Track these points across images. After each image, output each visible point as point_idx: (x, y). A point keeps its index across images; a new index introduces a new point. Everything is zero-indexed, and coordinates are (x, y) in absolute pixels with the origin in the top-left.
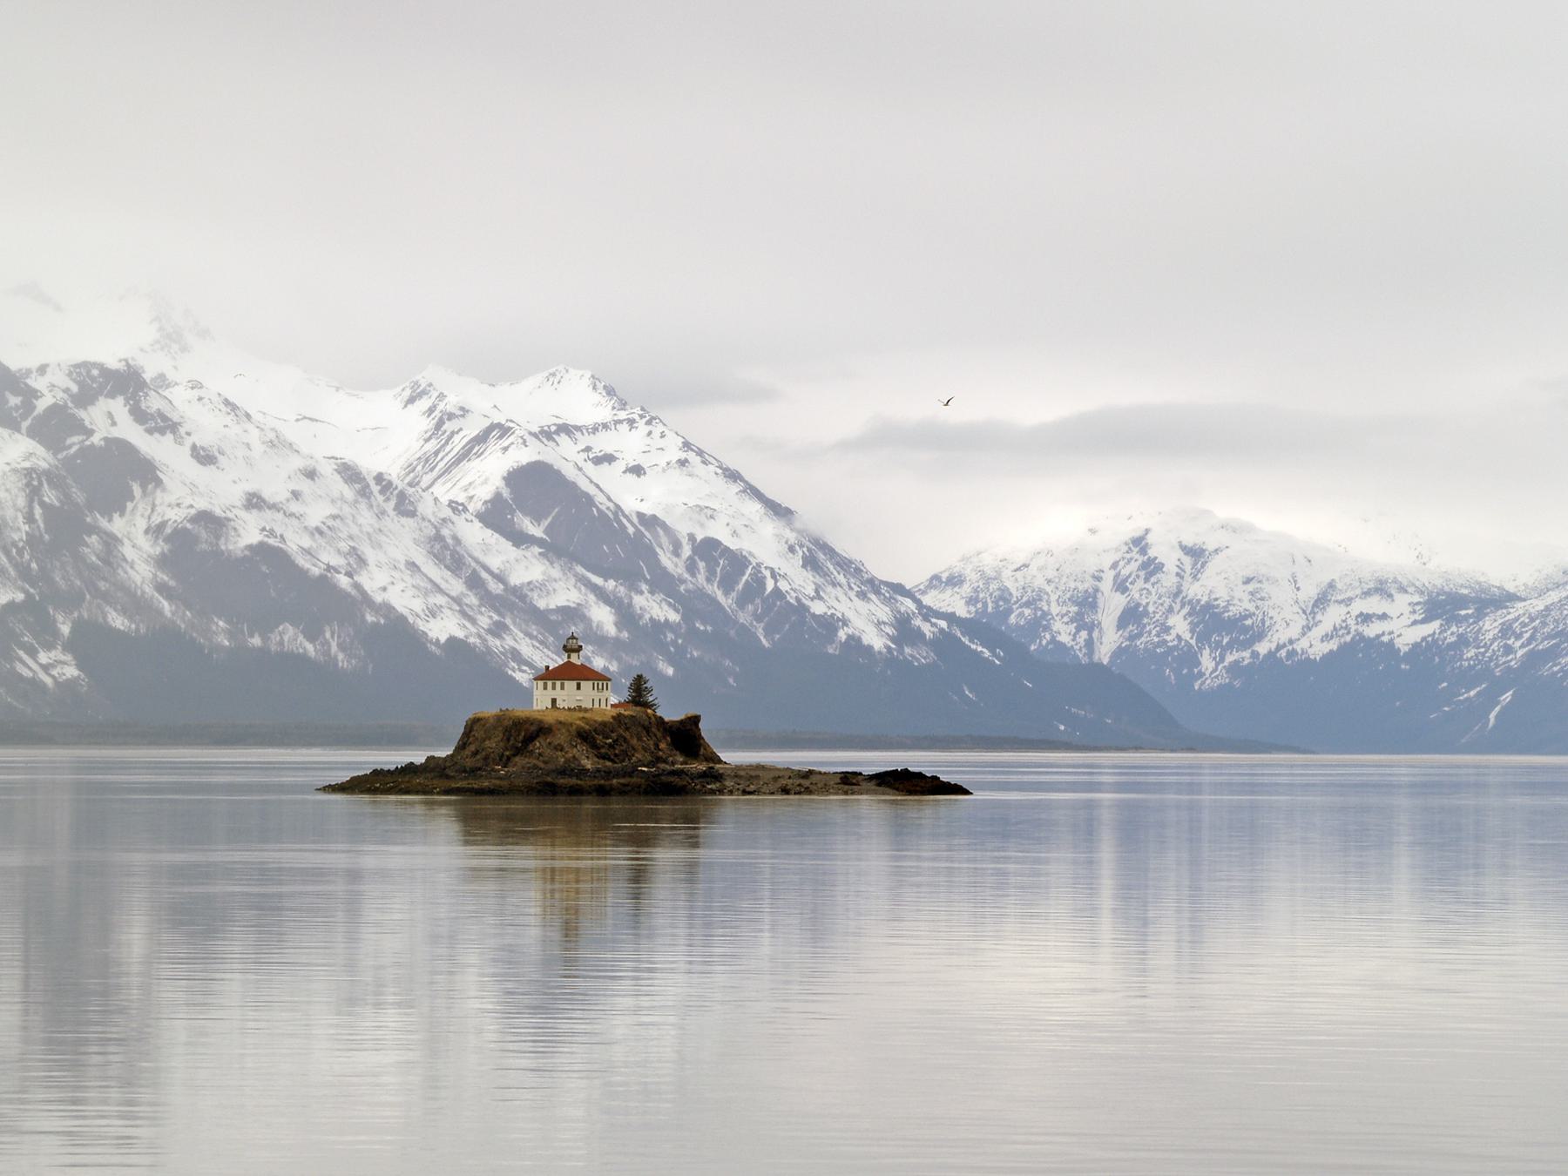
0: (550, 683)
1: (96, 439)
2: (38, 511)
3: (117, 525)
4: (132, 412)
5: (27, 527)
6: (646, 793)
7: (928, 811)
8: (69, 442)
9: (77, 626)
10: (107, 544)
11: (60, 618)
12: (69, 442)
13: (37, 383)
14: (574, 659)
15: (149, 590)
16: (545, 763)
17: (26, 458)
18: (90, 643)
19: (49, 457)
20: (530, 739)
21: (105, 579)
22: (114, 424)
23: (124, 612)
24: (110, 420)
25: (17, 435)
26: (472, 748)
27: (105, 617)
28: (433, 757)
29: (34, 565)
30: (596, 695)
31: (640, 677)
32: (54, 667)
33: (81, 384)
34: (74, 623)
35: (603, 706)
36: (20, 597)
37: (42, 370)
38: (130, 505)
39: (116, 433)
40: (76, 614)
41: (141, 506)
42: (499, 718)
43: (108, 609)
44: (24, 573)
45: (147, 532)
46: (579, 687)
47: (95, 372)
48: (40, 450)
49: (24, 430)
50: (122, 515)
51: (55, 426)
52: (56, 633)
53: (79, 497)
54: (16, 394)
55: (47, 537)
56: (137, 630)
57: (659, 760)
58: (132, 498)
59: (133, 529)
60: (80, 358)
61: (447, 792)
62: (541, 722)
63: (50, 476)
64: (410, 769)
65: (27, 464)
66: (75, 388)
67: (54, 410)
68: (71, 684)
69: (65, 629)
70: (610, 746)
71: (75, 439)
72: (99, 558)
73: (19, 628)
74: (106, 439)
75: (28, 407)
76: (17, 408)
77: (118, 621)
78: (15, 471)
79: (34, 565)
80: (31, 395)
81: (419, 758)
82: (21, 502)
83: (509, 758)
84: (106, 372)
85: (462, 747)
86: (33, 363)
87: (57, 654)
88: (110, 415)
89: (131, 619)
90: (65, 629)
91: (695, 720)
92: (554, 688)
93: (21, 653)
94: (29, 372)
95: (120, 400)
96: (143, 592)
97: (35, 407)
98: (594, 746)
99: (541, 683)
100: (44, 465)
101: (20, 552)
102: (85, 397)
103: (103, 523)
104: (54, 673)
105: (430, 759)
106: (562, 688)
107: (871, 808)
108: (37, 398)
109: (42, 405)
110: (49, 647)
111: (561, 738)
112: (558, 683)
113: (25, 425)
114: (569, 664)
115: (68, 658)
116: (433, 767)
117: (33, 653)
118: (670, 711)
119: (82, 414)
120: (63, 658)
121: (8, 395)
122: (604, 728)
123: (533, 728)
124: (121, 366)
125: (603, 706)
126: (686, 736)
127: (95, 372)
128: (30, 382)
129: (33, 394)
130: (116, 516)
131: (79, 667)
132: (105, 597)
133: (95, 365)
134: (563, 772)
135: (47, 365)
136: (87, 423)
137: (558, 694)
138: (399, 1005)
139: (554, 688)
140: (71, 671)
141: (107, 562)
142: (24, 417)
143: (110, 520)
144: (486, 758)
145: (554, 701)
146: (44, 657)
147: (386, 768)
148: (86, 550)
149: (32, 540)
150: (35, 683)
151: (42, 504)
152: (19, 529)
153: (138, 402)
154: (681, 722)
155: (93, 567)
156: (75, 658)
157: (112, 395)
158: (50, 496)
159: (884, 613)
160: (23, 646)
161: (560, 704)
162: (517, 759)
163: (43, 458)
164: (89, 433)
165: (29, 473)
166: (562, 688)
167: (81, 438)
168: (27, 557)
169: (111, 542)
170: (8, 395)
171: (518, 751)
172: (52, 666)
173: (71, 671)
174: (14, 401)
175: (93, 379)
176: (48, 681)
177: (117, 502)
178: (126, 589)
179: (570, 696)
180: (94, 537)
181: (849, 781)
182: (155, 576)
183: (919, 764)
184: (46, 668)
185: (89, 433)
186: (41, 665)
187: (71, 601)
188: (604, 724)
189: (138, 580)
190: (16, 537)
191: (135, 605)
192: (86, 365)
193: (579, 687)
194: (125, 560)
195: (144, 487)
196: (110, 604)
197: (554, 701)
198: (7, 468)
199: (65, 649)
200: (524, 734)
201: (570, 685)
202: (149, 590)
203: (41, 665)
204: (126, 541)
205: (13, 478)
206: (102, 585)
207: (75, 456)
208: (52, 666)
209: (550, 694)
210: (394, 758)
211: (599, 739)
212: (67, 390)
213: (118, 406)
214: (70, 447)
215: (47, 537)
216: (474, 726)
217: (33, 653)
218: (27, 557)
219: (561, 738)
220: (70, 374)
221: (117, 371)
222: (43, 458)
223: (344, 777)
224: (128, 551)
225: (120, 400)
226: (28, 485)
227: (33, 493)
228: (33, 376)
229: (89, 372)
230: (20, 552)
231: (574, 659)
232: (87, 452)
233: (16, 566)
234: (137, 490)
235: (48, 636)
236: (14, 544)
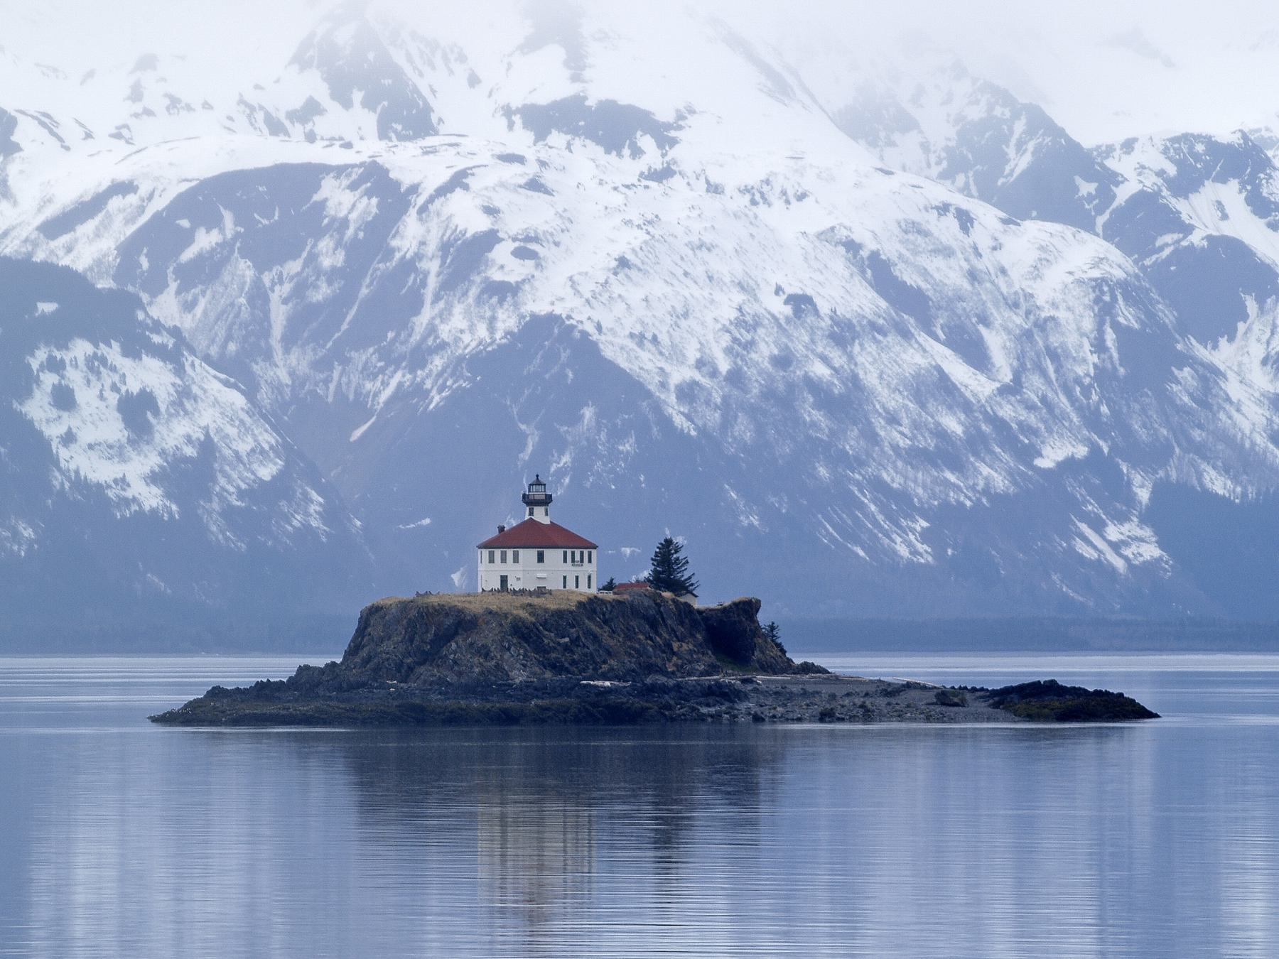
0: (498, 553)
1: (1196, 239)
2: (1110, 337)
3: (1223, 355)
4: (1249, 201)
5: (1094, 358)
6: (577, 720)
7: (1112, 745)
8: (1159, 243)
9: (1160, 490)
10: (1204, 380)
11: (1137, 479)
12: (1159, 243)
13: (1121, 164)
14: (540, 515)
15: (1261, 440)
16: (460, 674)
17: (1095, 266)
18: (1176, 512)
19: (1128, 264)
20: (445, 637)
21: (1200, 426)
22: (1225, 217)
23: (1226, 470)
24: (1218, 212)
25: (1084, 235)
26: (364, 653)
27: (1200, 476)
28: (307, 668)
29: (1104, 409)
30: (570, 570)
31: (669, 542)
32: (1126, 544)
33: (1180, 164)
34: (1155, 486)
36: (1082, 451)
37: (1129, 146)
38: (1241, 327)
39: (1228, 229)
40: (1161, 473)
41: (1256, 327)
42: (405, 606)
43: (1204, 466)
44: (1092, 420)
45: (1264, 362)
46: (541, 558)
47: (1200, 148)
48: (1115, 254)
49: (1099, 229)
50: (1231, 339)
51: (1141, 222)
52: (1131, 500)
53: (1167, 316)
54: (1089, 179)
55: (1122, 371)
56: (1244, 495)
57: (651, 669)
58: (1245, 317)
59: (1245, 359)
60: (1179, 130)
61: (236, 722)
62: (460, 611)
63: (1128, 290)
64: (264, 690)
65: (1096, 274)
66: (1172, 170)
67: (1143, 200)
68: (1151, 567)
69: (1144, 495)
70: (566, 648)
71: (1169, 238)
72: (1191, 395)
73: (1080, 493)
74: (1209, 238)
75: (1105, 196)
76: (1090, 198)
77: (1218, 483)
78: (1080, 282)
79: (1104, 409)
80: (1109, 180)
81: (281, 668)
82: (1088, 324)
83: (411, 669)
84: (1213, 146)
85: (352, 652)
86: (1116, 137)
87: (1131, 528)
88: (1220, 206)
89: (1236, 480)
90: (1144, 495)
92: (504, 560)
93: (1084, 527)
94: (1110, 150)
95: (1234, 184)
96: (1253, 444)
97: (1114, 197)
98: (540, 649)
100: (1119, 274)
101: (1086, 391)
102: (1186, 183)
103: (1202, 352)
104: (1128, 552)
105: (303, 670)
106: (516, 560)
107: (992, 745)
108: (1117, 184)
109: (1123, 194)
110: (1121, 518)
111: (488, 636)
112: (510, 553)
113: (1101, 220)
115: (1147, 532)
116: (305, 681)
117: (1099, 527)
119: (1180, 205)
120: (1139, 532)
121: (1079, 181)
122: (560, 620)
123: (449, 621)
124: (1236, 139)
126: (734, 634)
127: (1200, 148)
128: (1111, 164)
129: (1113, 179)
130: (1223, 342)
131: (1162, 545)
132: (1201, 451)
133: (1199, 138)
134: (470, 690)
135: (1135, 140)
136: (1184, 217)
137: (510, 569)
139: (504, 560)
140: (1150, 551)
141: (1204, 404)
142: (1100, 211)
143: (1215, 347)
144: (377, 669)
145: (504, 580)
146: (1113, 532)
148: (1175, 388)
149: (1103, 376)
150: (1101, 567)
151: (1116, 326)
152: (1084, 361)
153: (1256, 188)
154: (725, 610)
155: (1183, 411)
156: (1156, 534)
157: (1222, 179)
158: (1127, 315)
160: (1085, 518)
161: (513, 584)
162: (422, 669)
163: (1118, 264)
164: (1187, 229)
165: (1098, 284)
166: (516, 560)
167: (1176, 236)
168: (1095, 397)
169: (1210, 376)
170: (1079, 181)
171: (427, 658)
172: (1125, 543)
173: (1150, 551)
174: (1087, 188)
175: (1197, 157)
176: (1119, 564)
177: (1223, 323)
178: (1227, 438)
180: (1187, 370)
181: (949, 700)
182: (1270, 421)
183: (1129, 678)
184: (1116, 547)
185: (1187, 229)
186: (1110, 543)
187: (1153, 456)
188: (559, 614)
189: (1246, 426)
190: (1080, 371)
191: (1241, 460)
192: (1186, 138)
193: (541, 558)
194: (1228, 399)
195: (1261, 302)
196: (1205, 458)
197: (504, 580)
198: (1071, 279)
199: (1144, 520)
200: (434, 629)
201: (528, 555)
202: (1261, 440)
203: (1110, 543)
204: (1230, 375)
205: (1077, 291)
206: (1197, 435)
207: (1168, 261)
208: (1125, 543)
209: (499, 569)
210: (241, 670)
211: (549, 638)
212: (1161, 173)
213: (1231, 193)
214: (1161, 249)
215: (1122, 371)
216: (372, 614)
217: (1099, 527)
218: (1095, 397)
220: (1165, 151)
221: (1229, 146)
222: (1118, 264)
223: (177, 701)
224: (1233, 388)
225: (1234, 184)
226: (1097, 300)
227: (1105, 312)
228: (1117, 154)
229: (1191, 147)
230: (1086, 391)
231: (540, 515)
232: (1184, 255)
233: (1080, 410)
234: (1251, 306)
235: (1117, 501)
236: (1078, 381)
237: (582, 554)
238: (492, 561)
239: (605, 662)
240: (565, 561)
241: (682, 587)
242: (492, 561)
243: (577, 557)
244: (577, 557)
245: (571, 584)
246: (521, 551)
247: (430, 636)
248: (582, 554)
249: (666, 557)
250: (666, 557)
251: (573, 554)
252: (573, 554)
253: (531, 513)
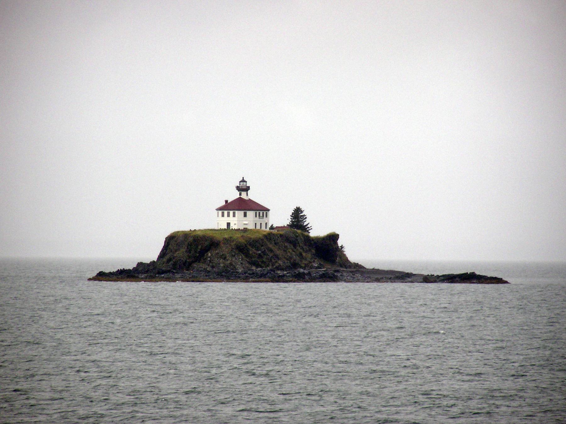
0: (226, 212)
14: (244, 195)
16: (213, 267)
35: (263, 228)
46: (245, 215)
70: (260, 256)
83: (190, 264)
91: (334, 237)
92: (228, 216)
98: (247, 255)
99: (220, 212)
106: (234, 216)
112: (231, 212)
114: (240, 200)
118: (318, 229)
123: (207, 243)
125: (263, 228)
138: (186, 261)
139: (228, 216)
147: (127, 268)
159: (73, 349)
166: (234, 216)
179: (238, 221)
193: (245, 215)
197: (228, 224)
201: (239, 214)
211: (252, 251)
219: (225, 249)
237: (263, 213)
238: (223, 216)
239: (276, 262)
240: (256, 216)
241: (305, 229)
242: (223, 216)
243: (261, 215)
244: (261, 215)
245: (258, 227)
246: (236, 212)
247: (199, 250)
248: (263, 213)
249: (297, 214)
250: (297, 214)
251: (259, 213)
252: (259, 213)
253: (240, 194)
